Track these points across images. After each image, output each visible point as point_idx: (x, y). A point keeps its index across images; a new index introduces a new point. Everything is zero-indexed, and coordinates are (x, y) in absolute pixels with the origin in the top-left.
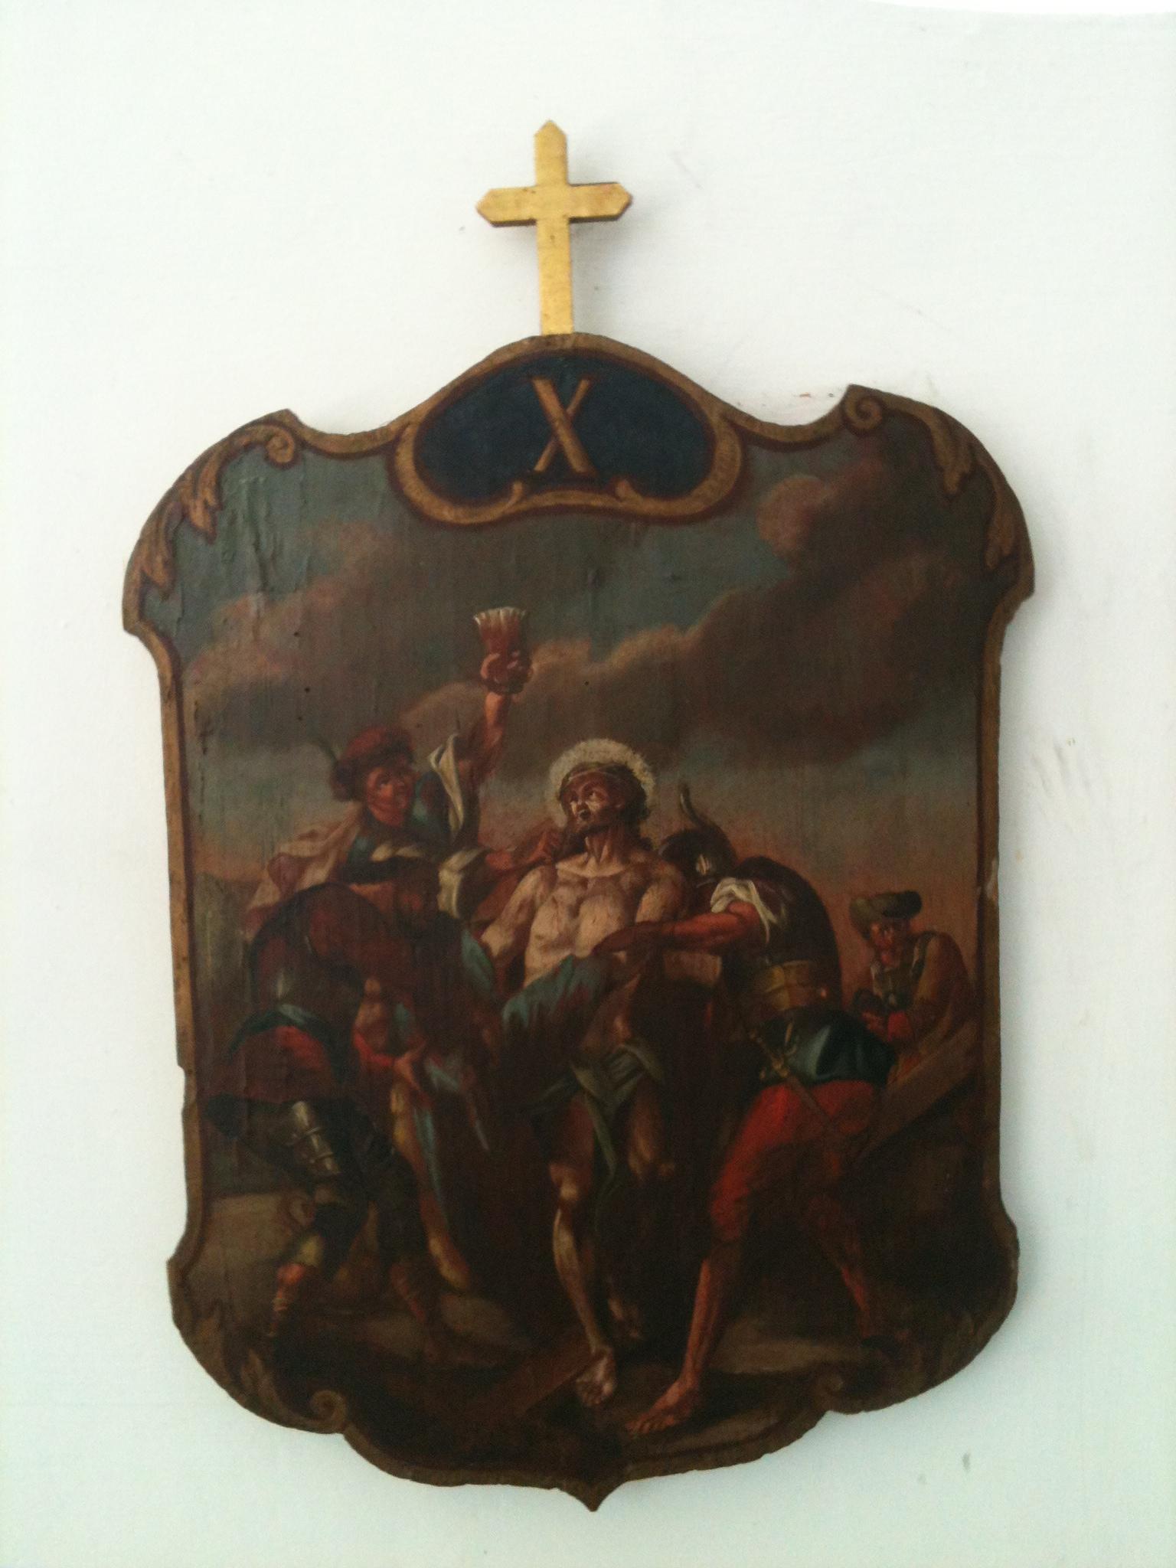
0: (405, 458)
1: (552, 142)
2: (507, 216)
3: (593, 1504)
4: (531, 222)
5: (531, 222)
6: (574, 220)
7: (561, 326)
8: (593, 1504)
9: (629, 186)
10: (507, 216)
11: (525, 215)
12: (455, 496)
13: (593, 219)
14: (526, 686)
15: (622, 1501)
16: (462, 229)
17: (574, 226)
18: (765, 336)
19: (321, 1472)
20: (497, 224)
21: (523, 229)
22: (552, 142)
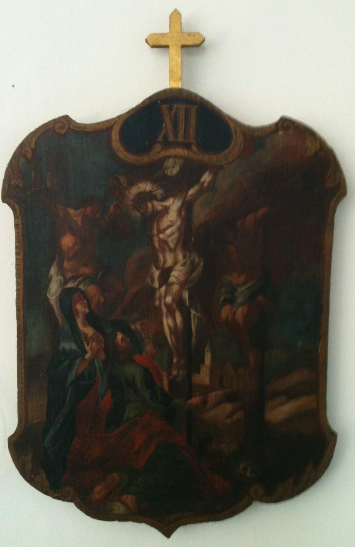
0: (115, 136)
1: (175, 16)
2: (158, 44)
3: (168, 534)
4: (167, 47)
5: (167, 47)
6: (183, 46)
7: (177, 85)
8: (168, 534)
9: (204, 34)
10: (158, 44)
11: (163, 43)
12: (128, 149)
13: (193, 46)
14: (36, 138)
15: (180, 534)
16: (13, 86)
17: (184, 49)
18: (251, 91)
19: (63, 517)
20: (153, 46)
21: (165, 49)
22: (175, 16)
